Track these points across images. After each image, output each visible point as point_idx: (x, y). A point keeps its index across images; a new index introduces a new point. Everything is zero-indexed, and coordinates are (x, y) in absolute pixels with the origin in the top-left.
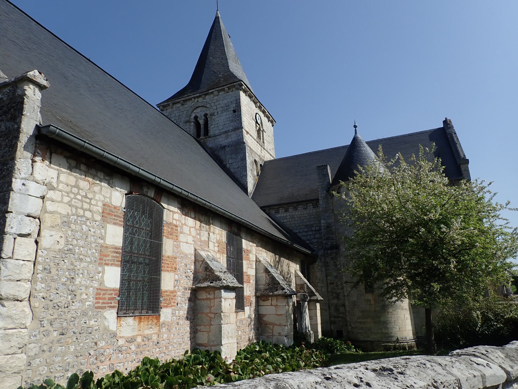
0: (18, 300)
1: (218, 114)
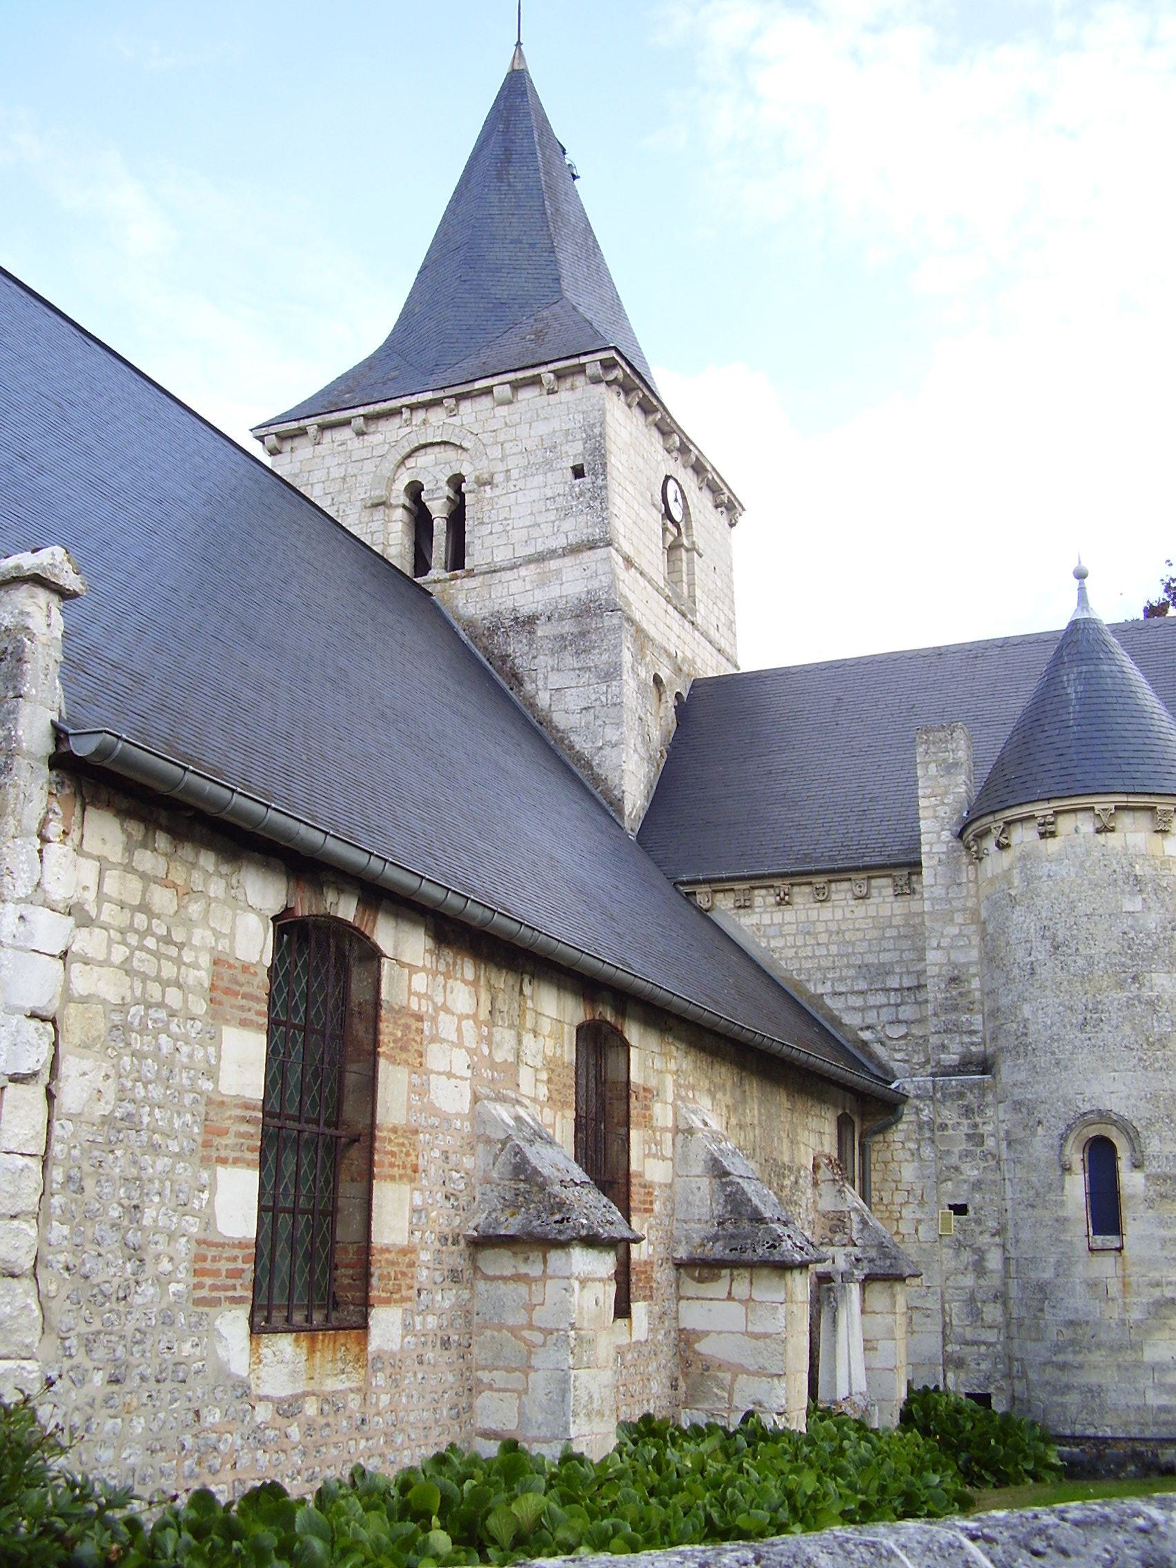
0: (13, 1276)
1: (508, 479)
